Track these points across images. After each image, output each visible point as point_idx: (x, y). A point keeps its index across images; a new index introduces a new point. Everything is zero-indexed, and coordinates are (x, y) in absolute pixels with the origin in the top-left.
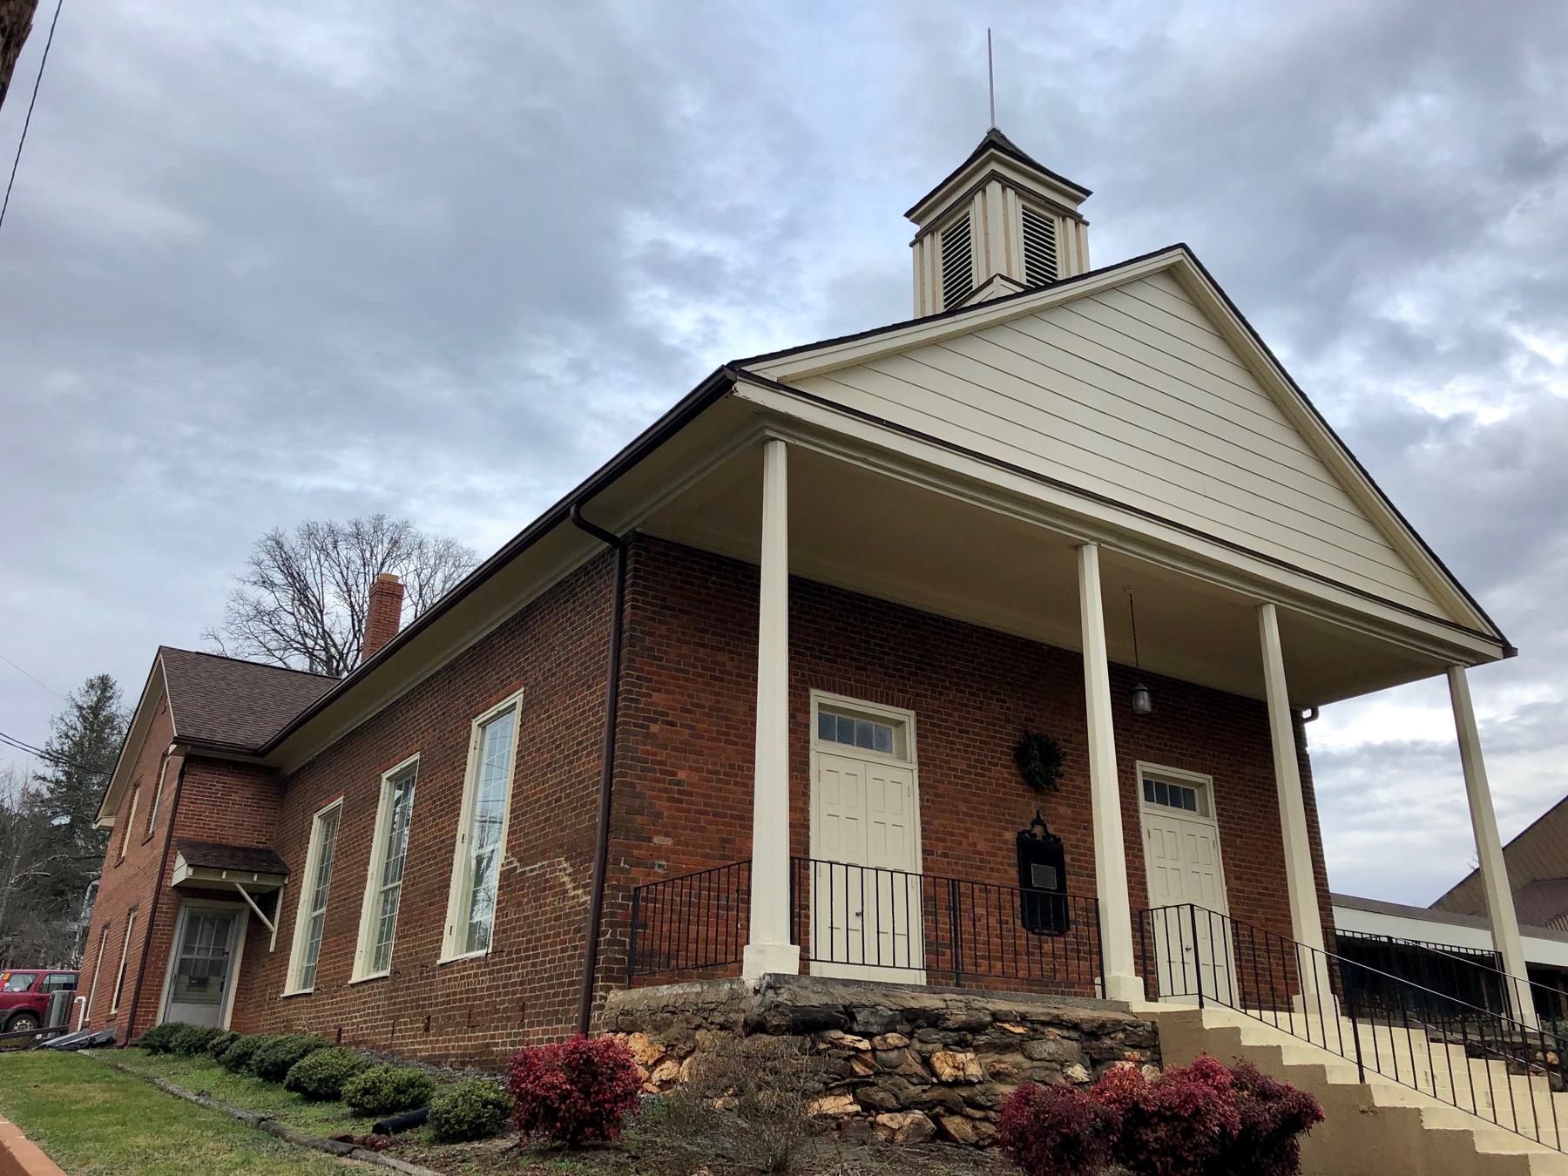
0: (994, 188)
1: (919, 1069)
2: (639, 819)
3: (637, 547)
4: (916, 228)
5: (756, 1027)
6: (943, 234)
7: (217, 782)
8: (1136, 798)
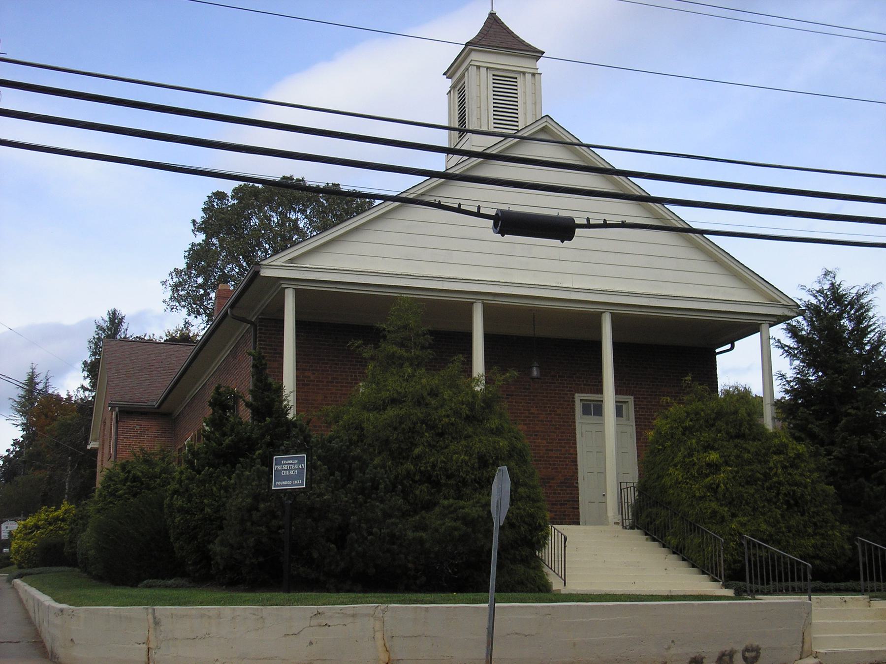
7: (137, 425)
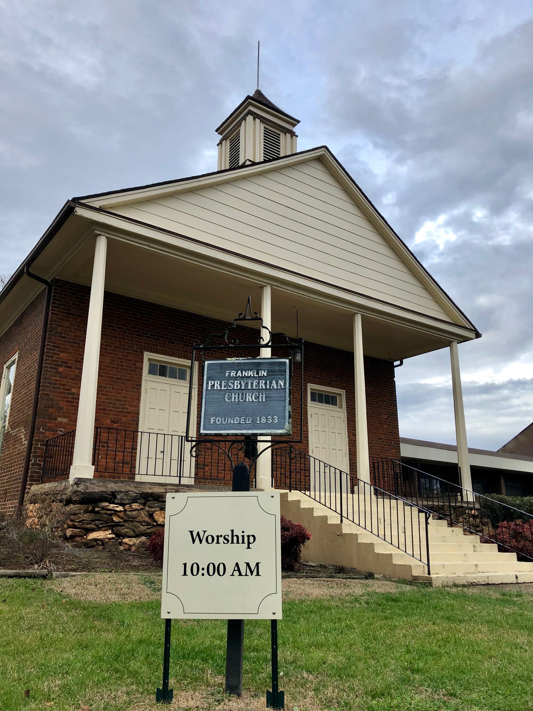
0: (250, 118)
1: (147, 519)
2: (51, 410)
3: (55, 286)
4: (221, 137)
5: (69, 502)
6: (230, 140)
8: (306, 400)
